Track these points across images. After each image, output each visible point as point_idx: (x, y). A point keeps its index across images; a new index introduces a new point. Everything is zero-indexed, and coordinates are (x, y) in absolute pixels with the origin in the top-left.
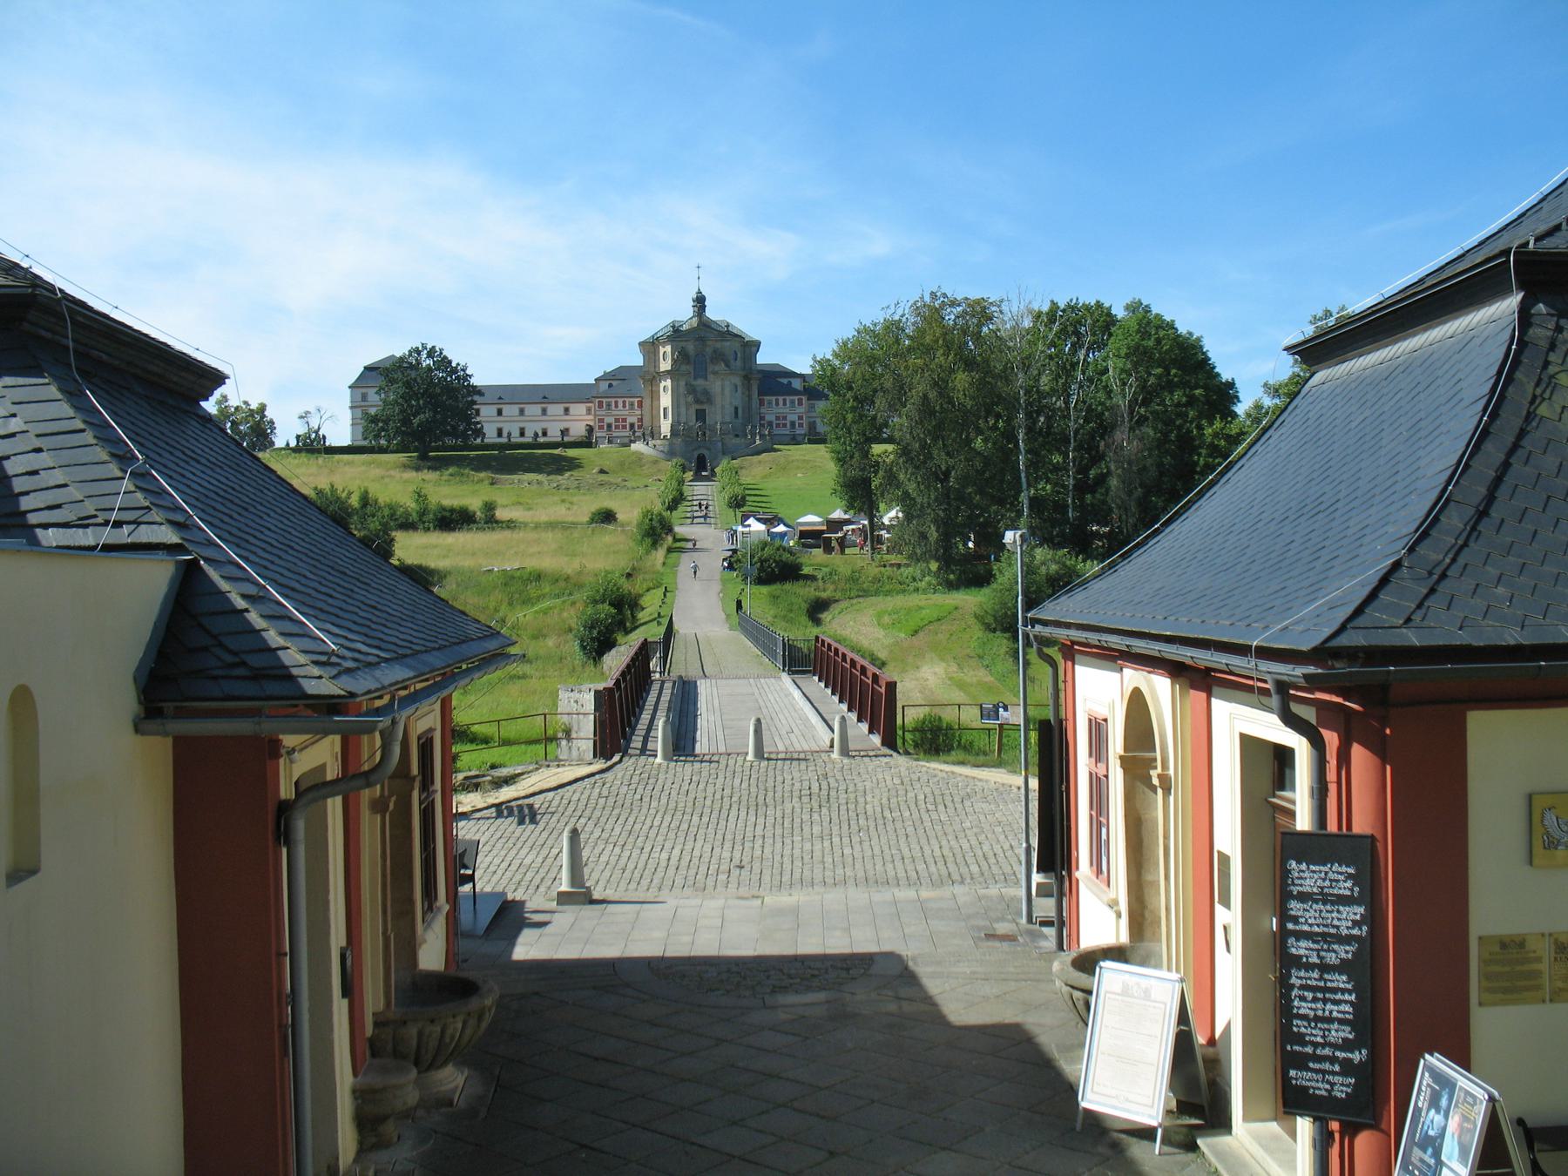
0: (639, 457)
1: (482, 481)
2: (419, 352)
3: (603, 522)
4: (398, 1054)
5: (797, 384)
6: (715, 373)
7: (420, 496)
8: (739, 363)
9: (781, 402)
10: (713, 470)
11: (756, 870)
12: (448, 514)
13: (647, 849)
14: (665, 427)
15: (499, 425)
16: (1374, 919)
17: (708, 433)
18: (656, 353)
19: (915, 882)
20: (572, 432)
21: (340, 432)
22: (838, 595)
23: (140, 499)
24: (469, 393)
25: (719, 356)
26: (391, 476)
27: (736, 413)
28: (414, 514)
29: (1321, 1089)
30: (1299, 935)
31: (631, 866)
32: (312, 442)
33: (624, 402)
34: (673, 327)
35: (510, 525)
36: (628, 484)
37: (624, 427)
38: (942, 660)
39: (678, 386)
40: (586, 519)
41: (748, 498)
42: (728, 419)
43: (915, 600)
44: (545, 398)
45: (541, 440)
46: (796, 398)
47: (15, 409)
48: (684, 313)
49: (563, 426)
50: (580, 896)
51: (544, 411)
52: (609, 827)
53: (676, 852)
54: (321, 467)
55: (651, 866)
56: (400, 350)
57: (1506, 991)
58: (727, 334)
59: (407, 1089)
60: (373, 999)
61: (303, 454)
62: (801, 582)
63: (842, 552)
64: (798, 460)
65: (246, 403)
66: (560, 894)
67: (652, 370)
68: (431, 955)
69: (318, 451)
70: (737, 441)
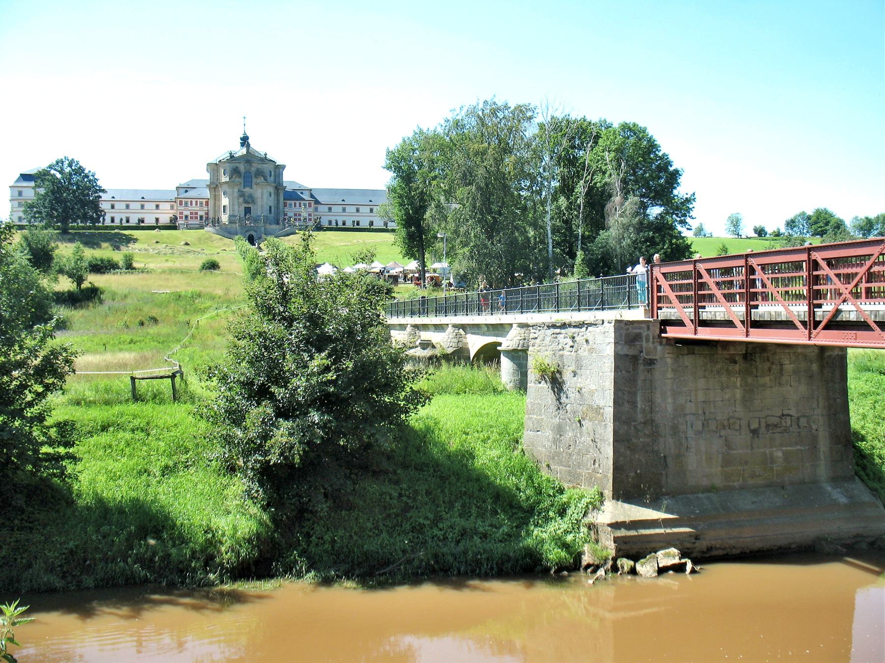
6: (257, 184)
8: (272, 178)
9: (298, 205)
12: (99, 263)
18: (218, 171)
25: (259, 173)
33: (196, 202)
34: (231, 154)
37: (196, 218)
44: (143, 198)
49: (140, 216)
58: (265, 160)
67: (215, 181)
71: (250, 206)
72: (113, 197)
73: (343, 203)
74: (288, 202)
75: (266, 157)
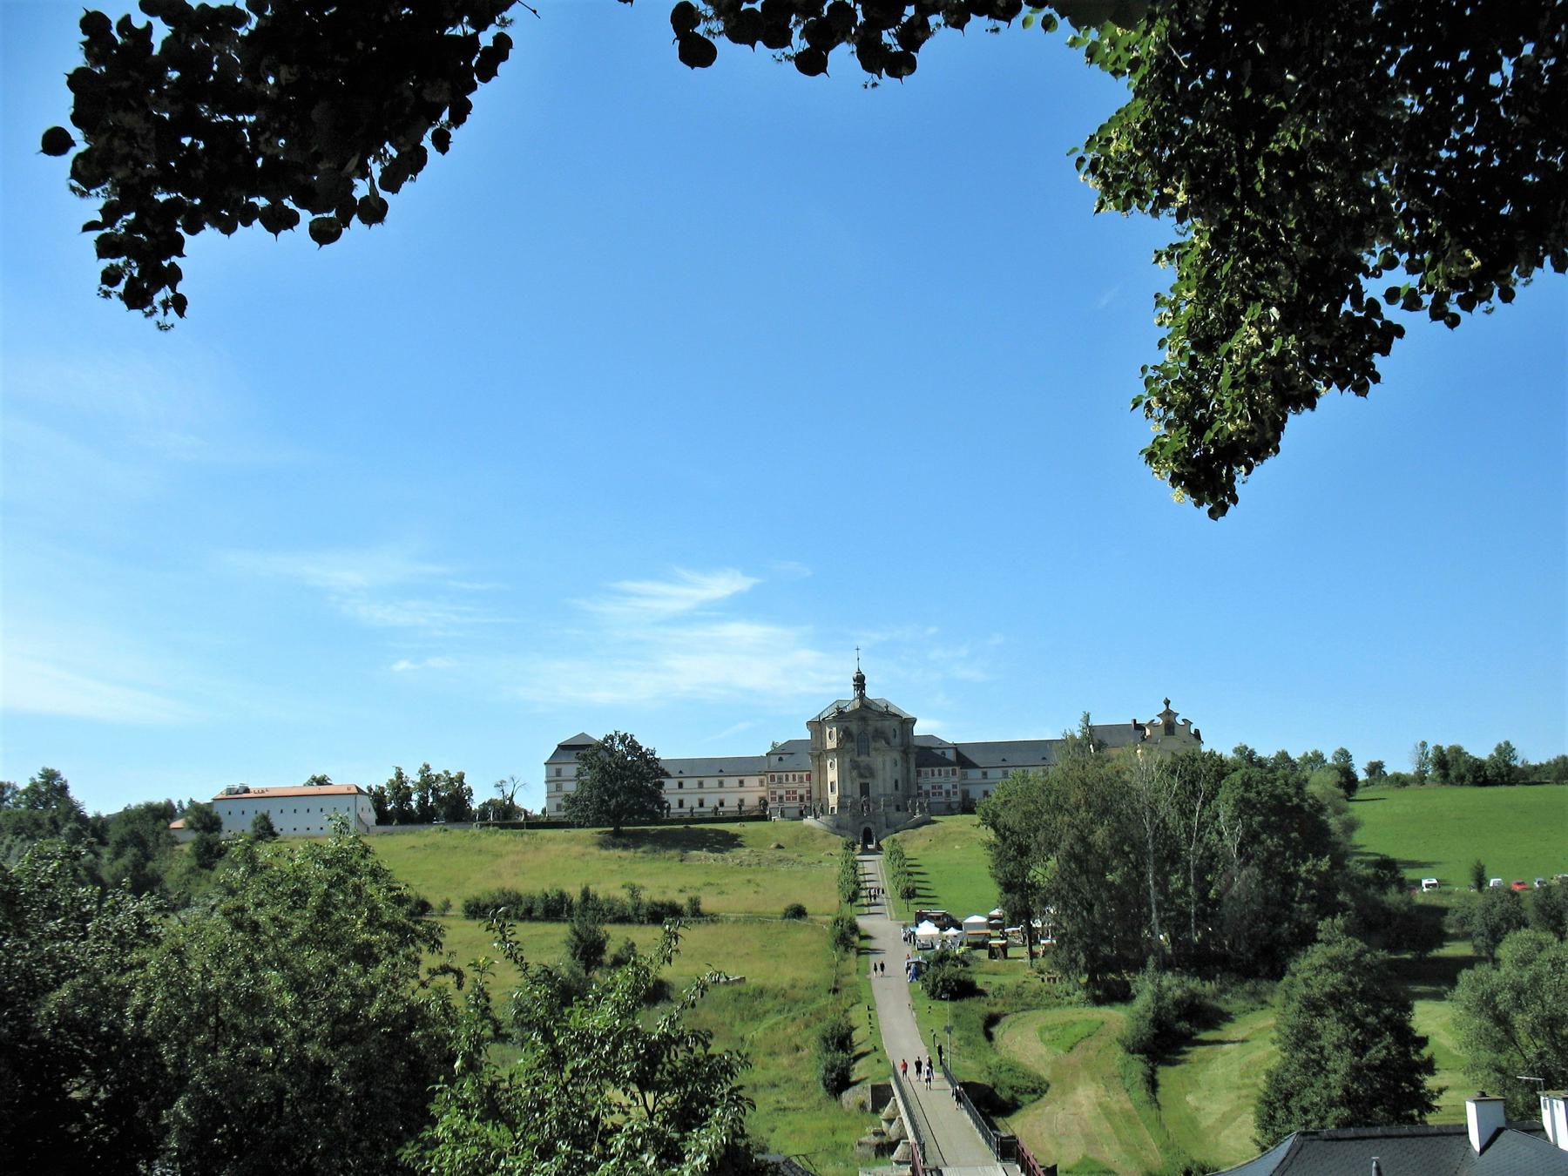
2: (612, 738)
3: (794, 917)
5: (951, 755)
6: (876, 750)
7: (634, 891)
8: (898, 740)
9: (936, 772)
12: (659, 909)
14: (833, 799)
17: (871, 805)
18: (822, 732)
21: (534, 800)
22: (1006, 1009)
25: (879, 734)
26: (591, 854)
27: (896, 786)
28: (630, 909)
33: (794, 776)
34: (838, 709)
35: (713, 918)
36: (805, 860)
37: (795, 798)
38: (1093, 1079)
39: (843, 762)
42: (889, 791)
46: (950, 768)
51: (721, 784)
54: (527, 844)
58: (887, 714)
62: (977, 998)
64: (954, 832)
65: (447, 772)
67: (819, 746)
71: (867, 781)
73: (1004, 764)
74: (923, 769)
75: (887, 711)
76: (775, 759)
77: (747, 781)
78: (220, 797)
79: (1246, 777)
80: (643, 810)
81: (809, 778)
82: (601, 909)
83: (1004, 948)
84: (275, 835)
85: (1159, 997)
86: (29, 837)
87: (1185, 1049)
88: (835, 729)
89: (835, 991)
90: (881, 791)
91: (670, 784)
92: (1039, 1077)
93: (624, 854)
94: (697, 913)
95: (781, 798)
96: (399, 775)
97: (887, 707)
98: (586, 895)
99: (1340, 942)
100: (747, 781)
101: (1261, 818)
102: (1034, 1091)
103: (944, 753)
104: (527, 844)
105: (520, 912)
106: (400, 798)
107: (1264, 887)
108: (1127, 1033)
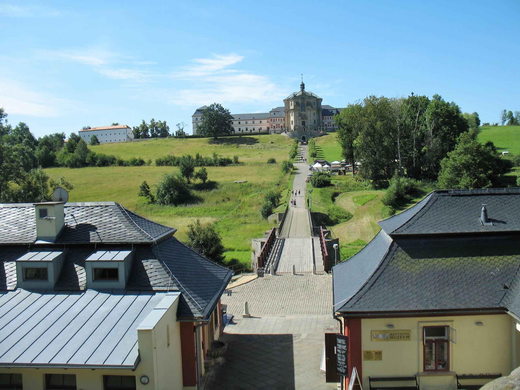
0: (284, 137)
1: (234, 147)
2: (213, 106)
4: (211, 356)
6: (308, 109)
7: (215, 155)
8: (315, 106)
9: (329, 118)
10: (307, 141)
11: (286, 309)
12: (223, 161)
13: (264, 302)
14: (292, 127)
15: (239, 127)
16: (347, 348)
18: (289, 103)
19: (318, 313)
20: (263, 129)
21: (189, 131)
22: (342, 191)
23: (172, 281)
24: (230, 118)
25: (309, 104)
27: (315, 122)
28: (213, 161)
29: (341, 371)
30: (339, 349)
31: (260, 307)
32: (181, 133)
33: (279, 119)
34: (294, 95)
35: (243, 164)
37: (279, 127)
38: (371, 214)
39: (296, 114)
40: (267, 161)
41: (317, 154)
42: (312, 124)
43: (366, 192)
45: (253, 132)
47: (152, 263)
48: (298, 90)
50: (248, 316)
51: (254, 122)
52: (257, 295)
53: (270, 303)
55: (264, 307)
56: (208, 105)
57: (367, 359)
58: (312, 97)
59: (212, 362)
60: (207, 347)
61: (178, 139)
62: (331, 187)
63: (345, 174)
65: (160, 121)
66: (244, 316)
67: (288, 108)
68: (216, 337)
69: (183, 138)
70: (315, 132)
72: (239, 118)
76: (272, 113)
77: (263, 121)
78: (81, 131)
79: (437, 104)
80: (225, 131)
81: (284, 120)
82: (203, 161)
83: (344, 171)
84: (99, 143)
85: (399, 185)
86: (11, 144)
87: (408, 204)
88: (293, 102)
89: (278, 185)
90: (309, 124)
91: (235, 123)
92: (349, 213)
93: (217, 145)
94: (237, 162)
95: (274, 127)
96: (144, 123)
97: (311, 94)
98: (198, 156)
99: (470, 142)
100: (263, 121)
101: (442, 119)
102: (346, 218)
103: (332, 111)
104: (184, 143)
105: (175, 163)
106: (144, 130)
107: (442, 146)
108: (385, 198)
